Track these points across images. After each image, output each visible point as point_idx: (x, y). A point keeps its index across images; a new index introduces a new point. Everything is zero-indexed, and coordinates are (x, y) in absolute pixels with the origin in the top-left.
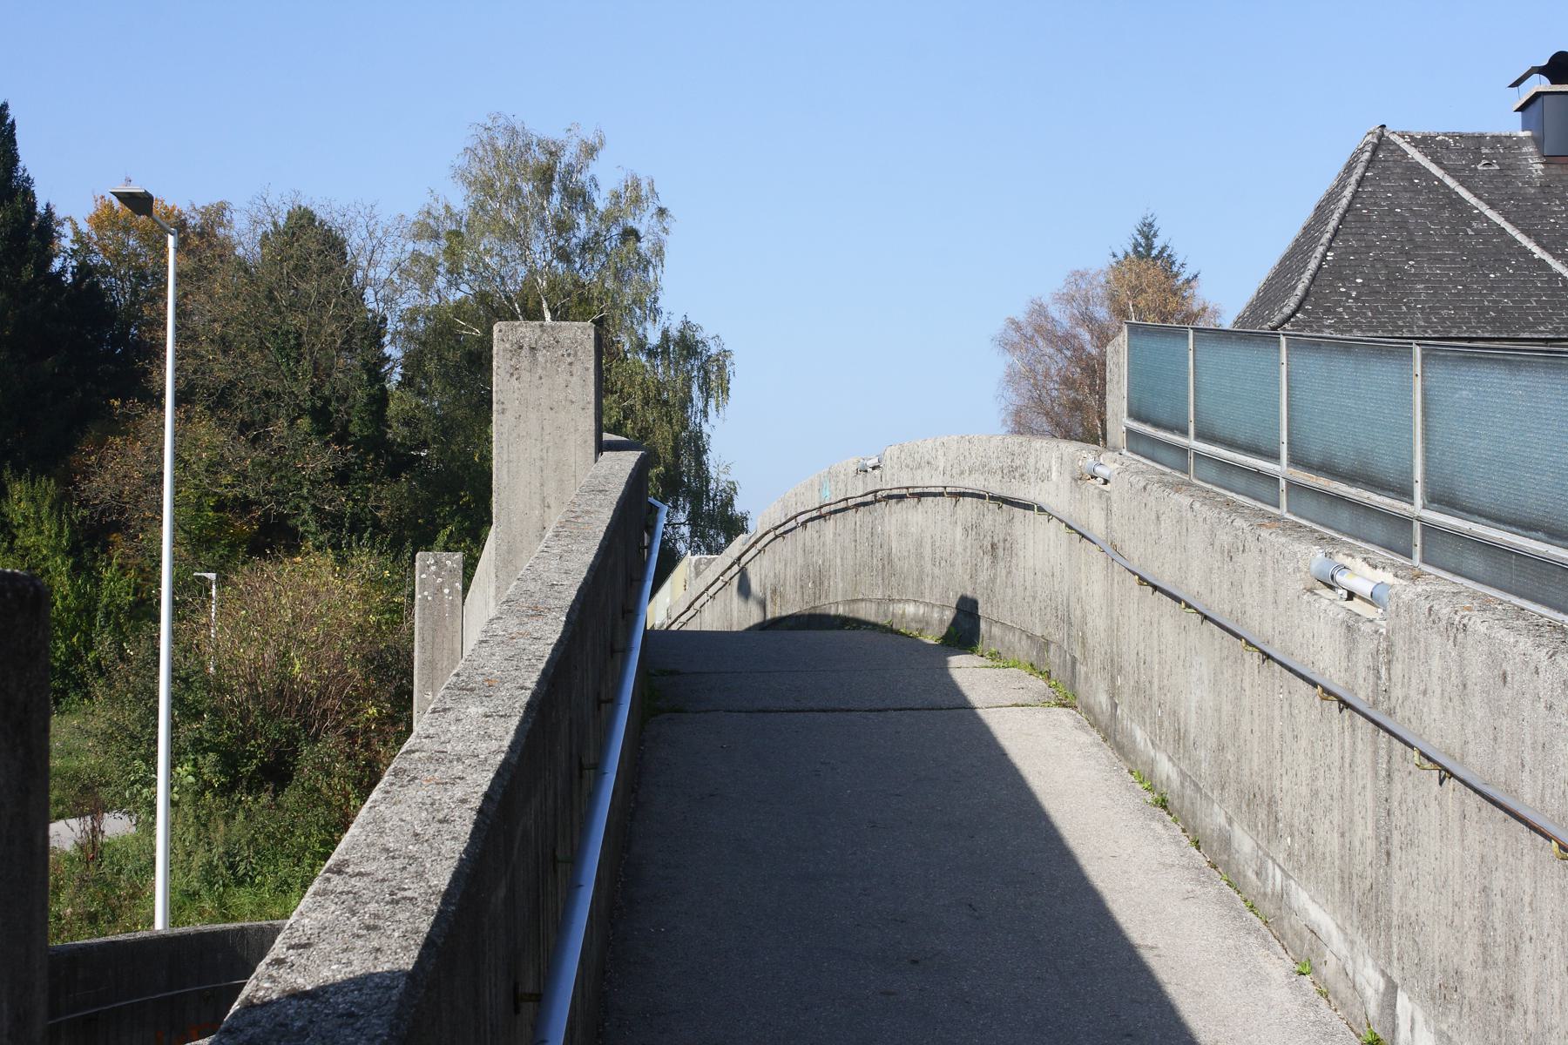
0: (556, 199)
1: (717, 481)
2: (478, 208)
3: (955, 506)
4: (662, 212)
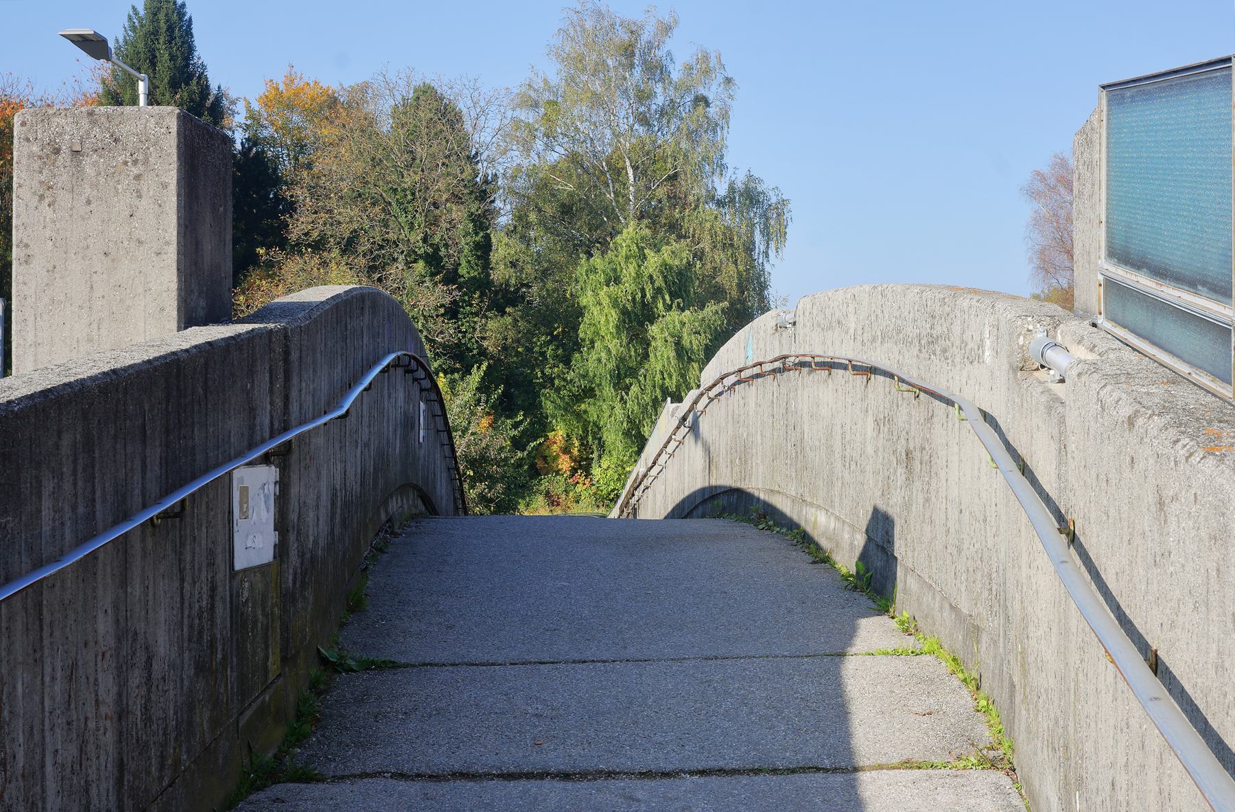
0: (638, 71)
2: (570, 81)
3: (866, 386)
4: (728, 81)
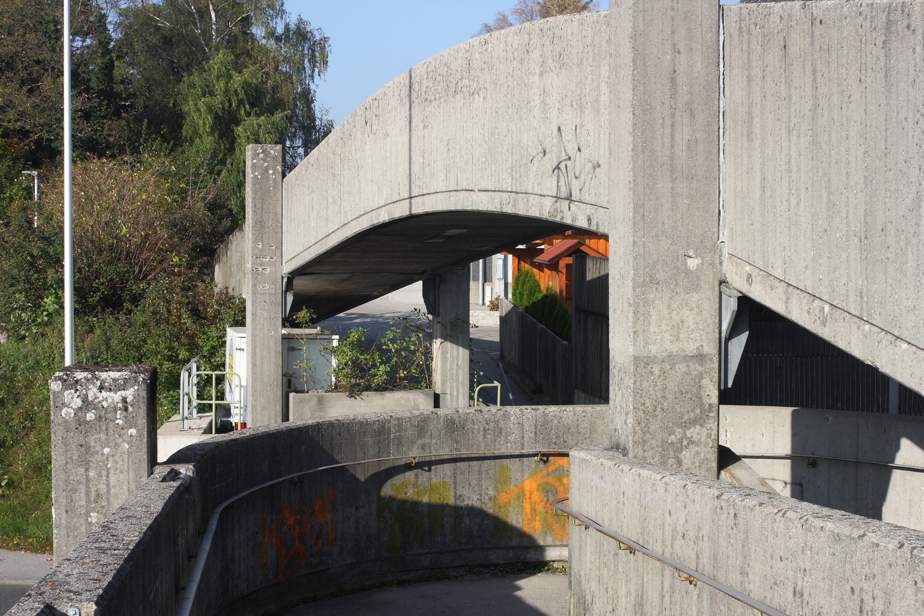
1: (321, 120)
